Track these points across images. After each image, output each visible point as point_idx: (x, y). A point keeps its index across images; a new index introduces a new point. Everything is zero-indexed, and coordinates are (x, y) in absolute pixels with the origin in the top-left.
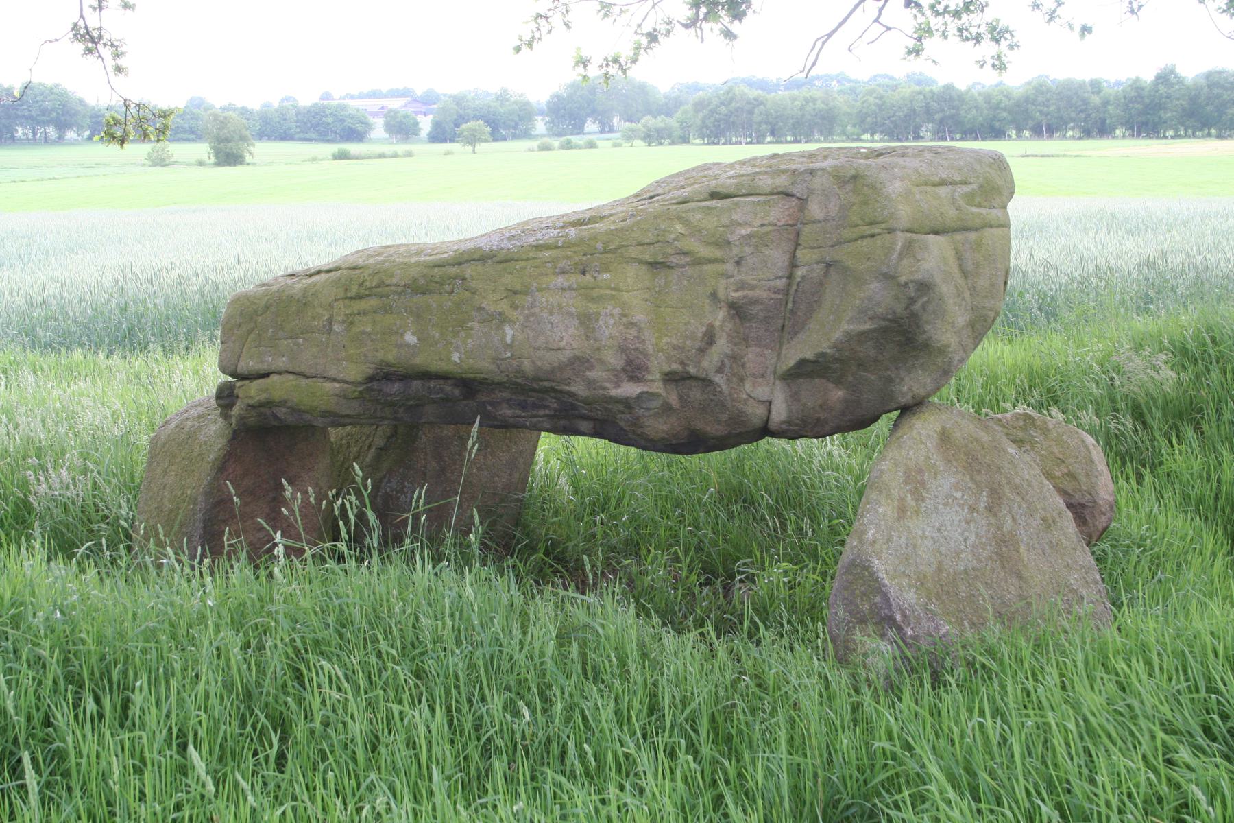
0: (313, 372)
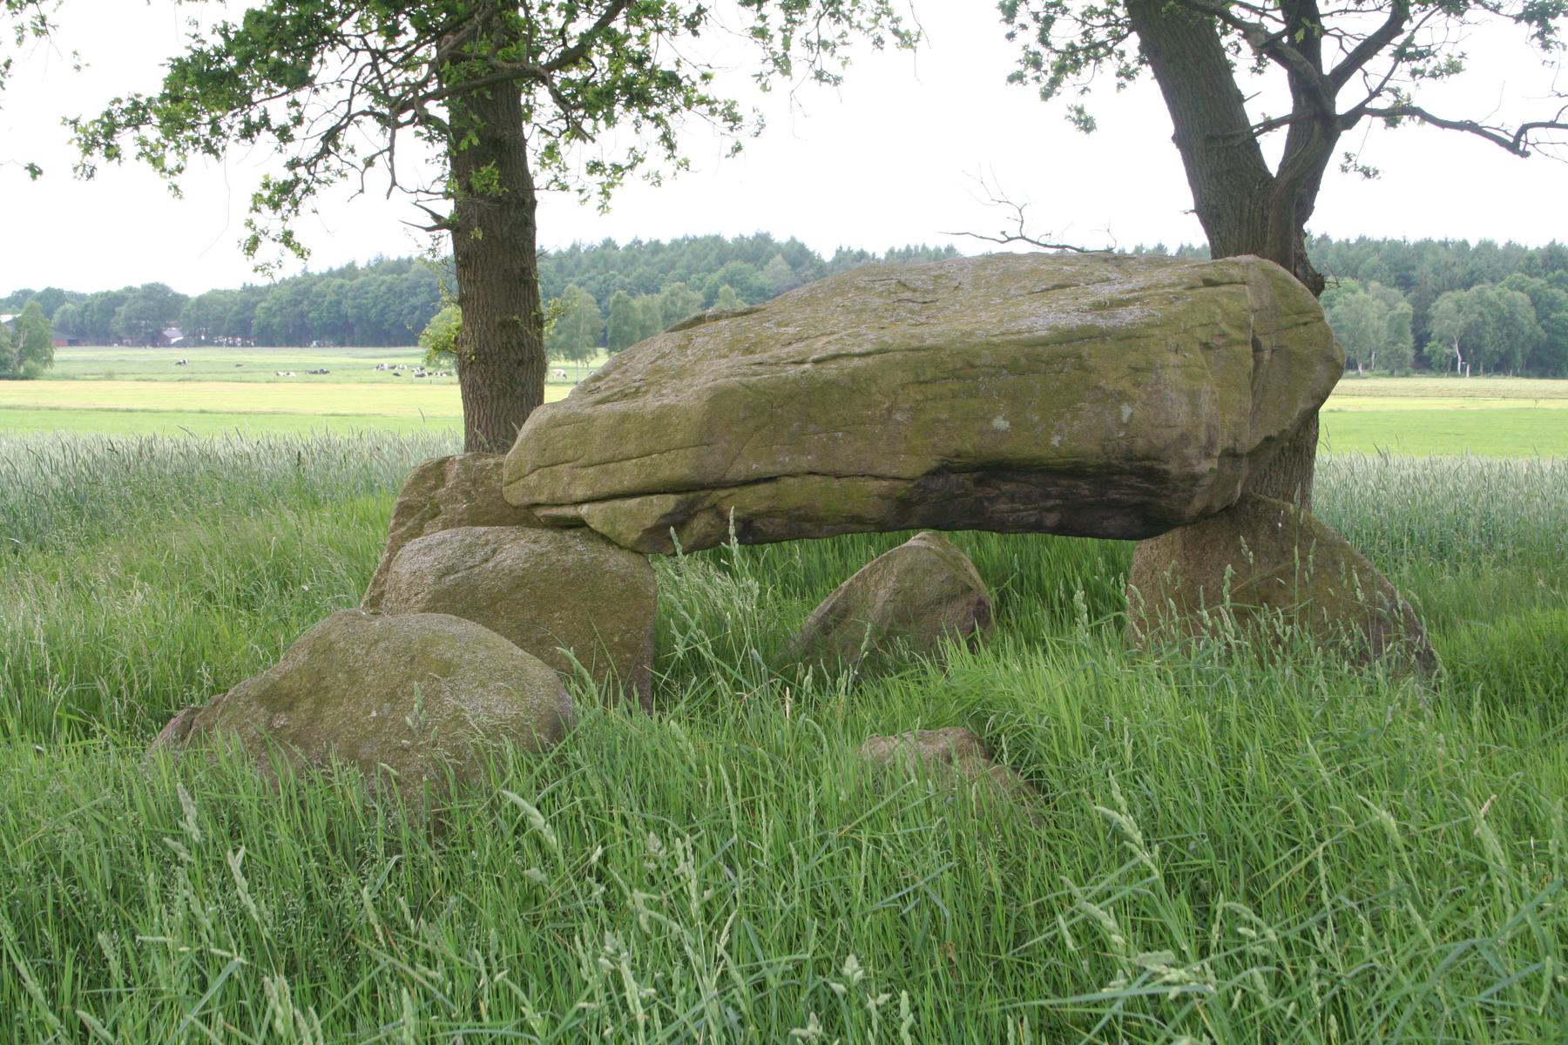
0: (853, 470)
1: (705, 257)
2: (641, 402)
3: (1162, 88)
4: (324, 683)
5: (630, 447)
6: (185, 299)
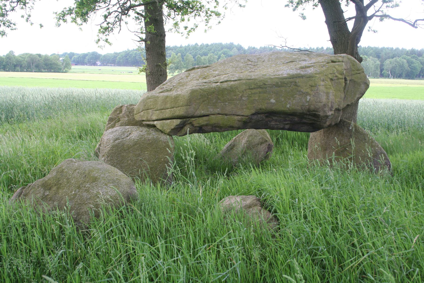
0: (231, 113)
1: (218, 48)
2: (171, 93)
3: (323, 9)
4: (60, 182)
5: (168, 106)
6: (101, 55)
